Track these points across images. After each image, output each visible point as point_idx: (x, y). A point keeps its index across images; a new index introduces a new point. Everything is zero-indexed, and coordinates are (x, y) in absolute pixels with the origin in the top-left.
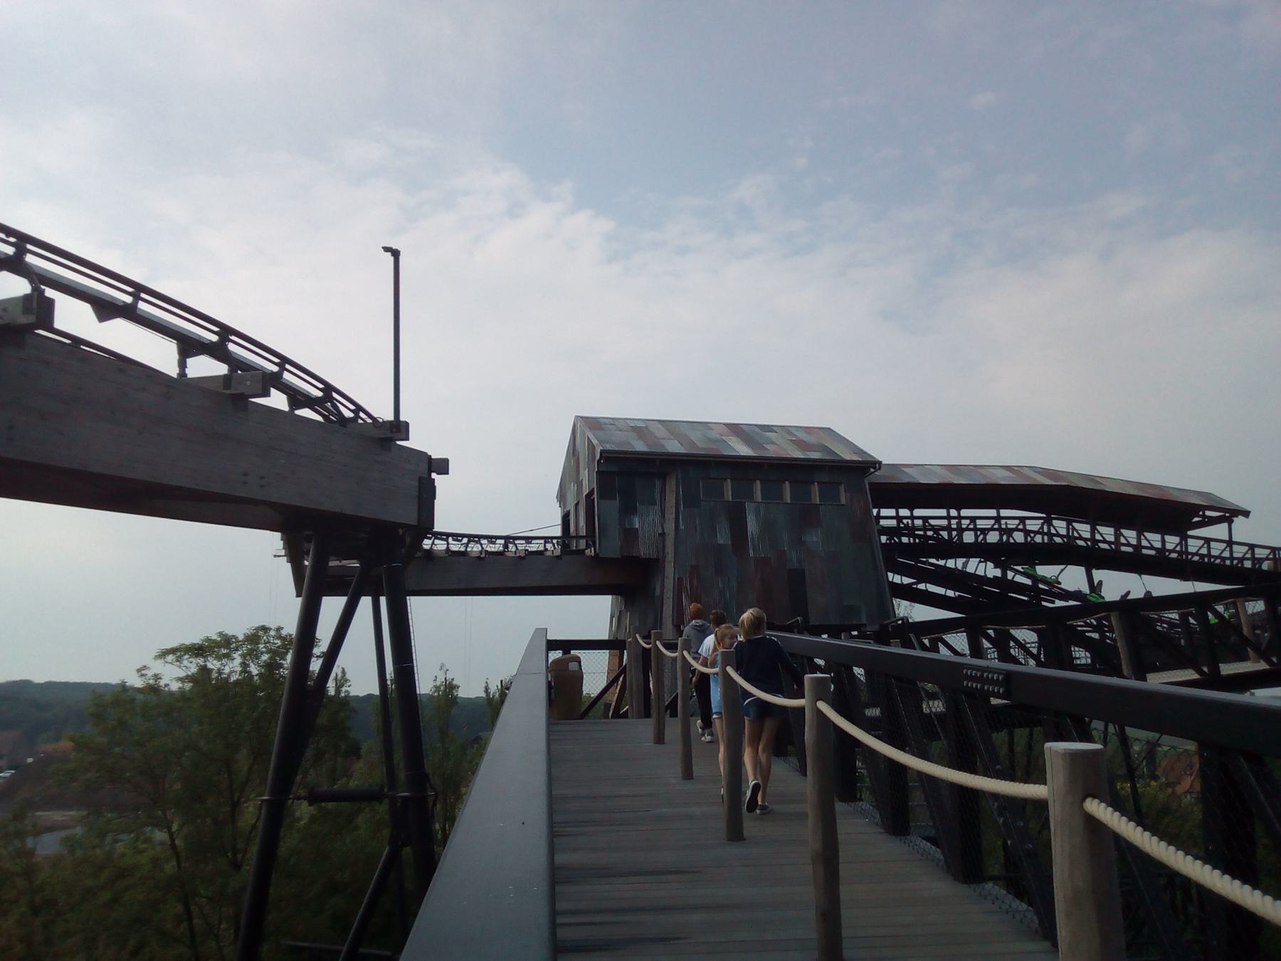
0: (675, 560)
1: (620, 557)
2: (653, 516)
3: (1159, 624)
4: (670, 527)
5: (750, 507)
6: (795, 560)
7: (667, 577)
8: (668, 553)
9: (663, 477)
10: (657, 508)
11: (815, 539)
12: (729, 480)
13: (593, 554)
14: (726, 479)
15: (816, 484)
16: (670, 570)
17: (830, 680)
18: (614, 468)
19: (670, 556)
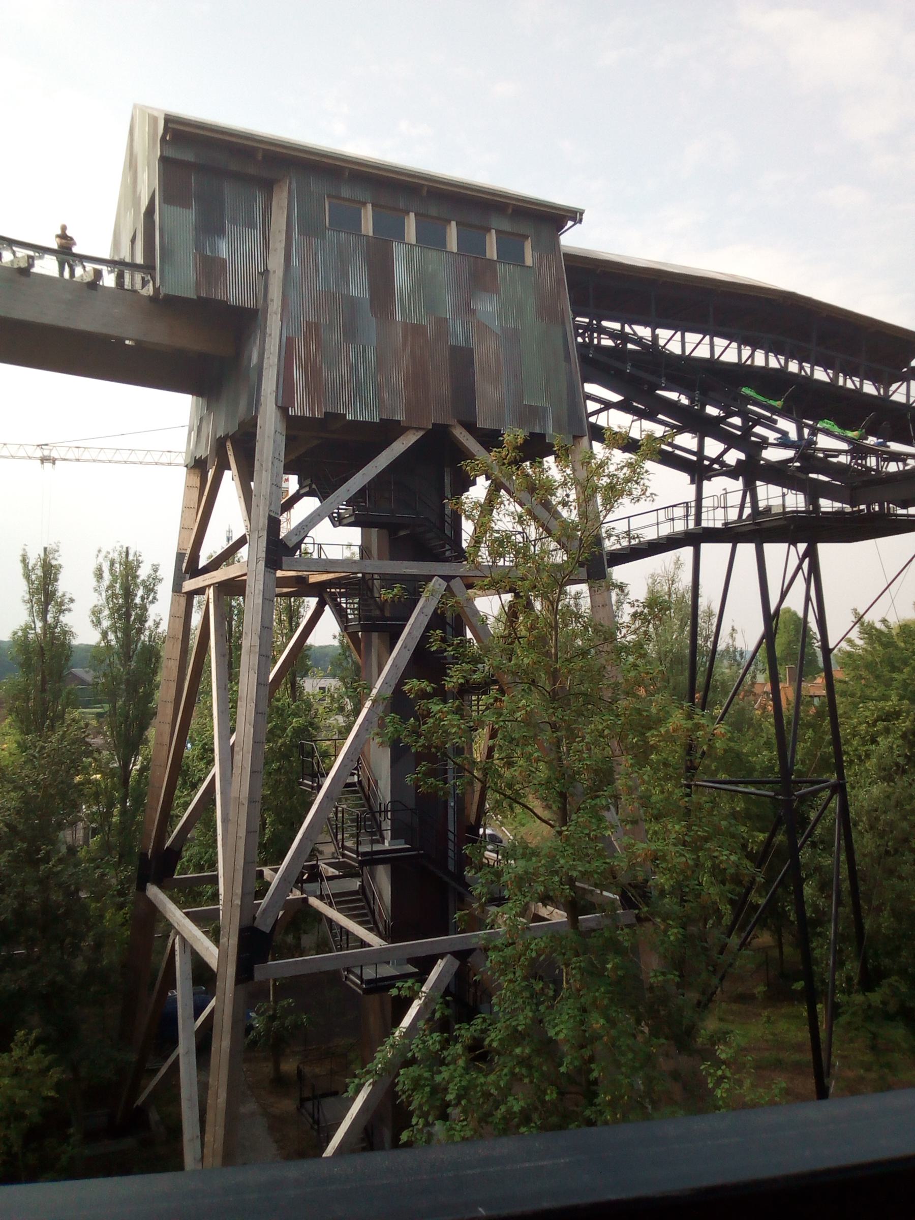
0: (282, 310)
1: (195, 297)
2: (251, 241)
3: (826, 505)
4: (276, 263)
5: (399, 251)
6: (459, 329)
7: (270, 335)
8: (272, 300)
9: (268, 186)
10: (258, 233)
11: (489, 308)
12: (369, 206)
13: (151, 292)
14: (364, 204)
15: (493, 231)
16: (274, 324)
17: (537, 430)
18: (188, 156)
19: (275, 307)
